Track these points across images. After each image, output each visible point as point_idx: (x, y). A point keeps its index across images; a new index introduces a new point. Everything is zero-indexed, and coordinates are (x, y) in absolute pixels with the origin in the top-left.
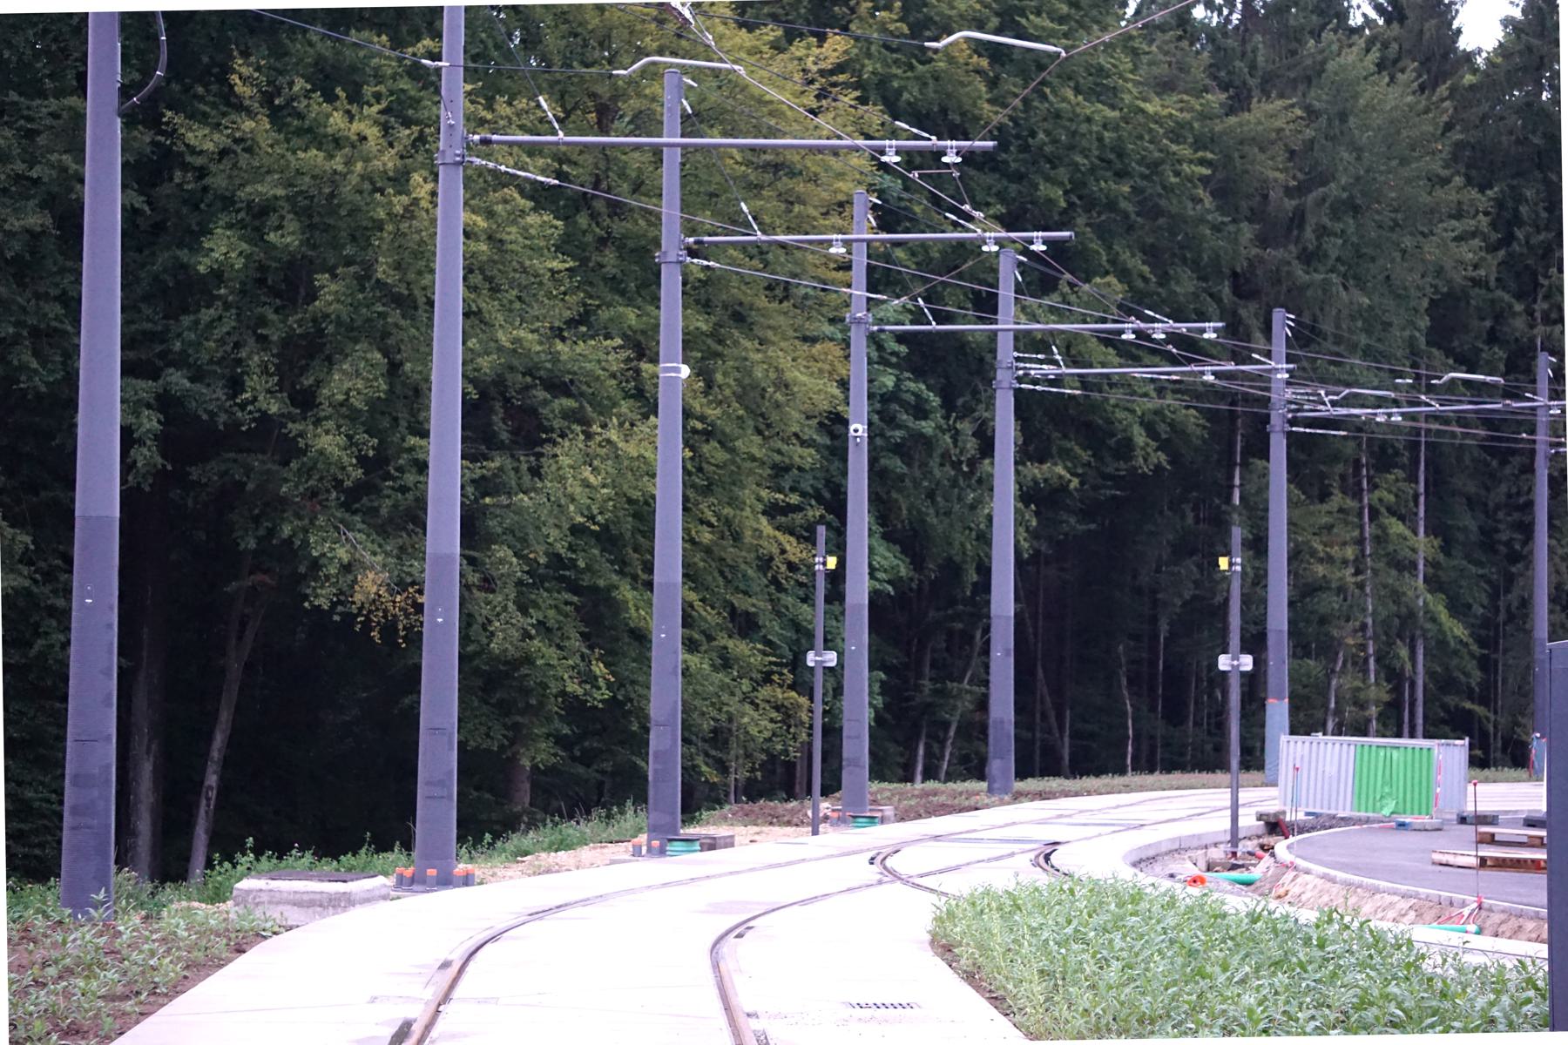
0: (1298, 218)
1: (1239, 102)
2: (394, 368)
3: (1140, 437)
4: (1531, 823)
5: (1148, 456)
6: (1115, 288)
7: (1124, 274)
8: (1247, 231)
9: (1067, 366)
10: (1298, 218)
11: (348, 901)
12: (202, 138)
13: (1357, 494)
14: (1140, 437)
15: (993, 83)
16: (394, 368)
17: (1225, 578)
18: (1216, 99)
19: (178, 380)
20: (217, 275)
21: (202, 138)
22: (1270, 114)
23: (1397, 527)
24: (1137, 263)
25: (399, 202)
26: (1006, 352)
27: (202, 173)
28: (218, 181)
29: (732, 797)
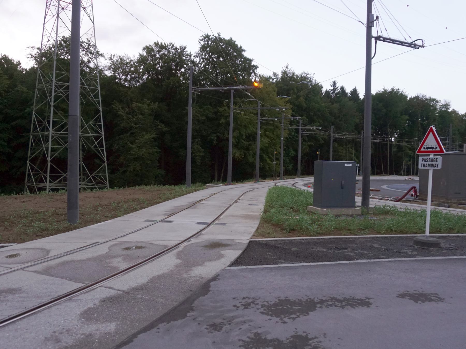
0: (339, 116)
1: (333, 104)
2: (240, 133)
3: (321, 140)
4: (357, 183)
5: (322, 142)
6: (318, 124)
7: (319, 122)
8: (333, 118)
9: (55, 96)
10: (339, 116)
11: (217, 186)
12: (221, 109)
13: (346, 146)
14: (321, 140)
15: (305, 102)
16: (240, 133)
17: (318, 154)
18: (330, 104)
19: (218, 134)
20: (222, 123)
21: (221, 109)
22: (336, 105)
23: (350, 149)
24: (321, 121)
25: (240, 116)
26: (300, 130)
27: (221, 113)
28: (223, 114)
29: (216, 179)
